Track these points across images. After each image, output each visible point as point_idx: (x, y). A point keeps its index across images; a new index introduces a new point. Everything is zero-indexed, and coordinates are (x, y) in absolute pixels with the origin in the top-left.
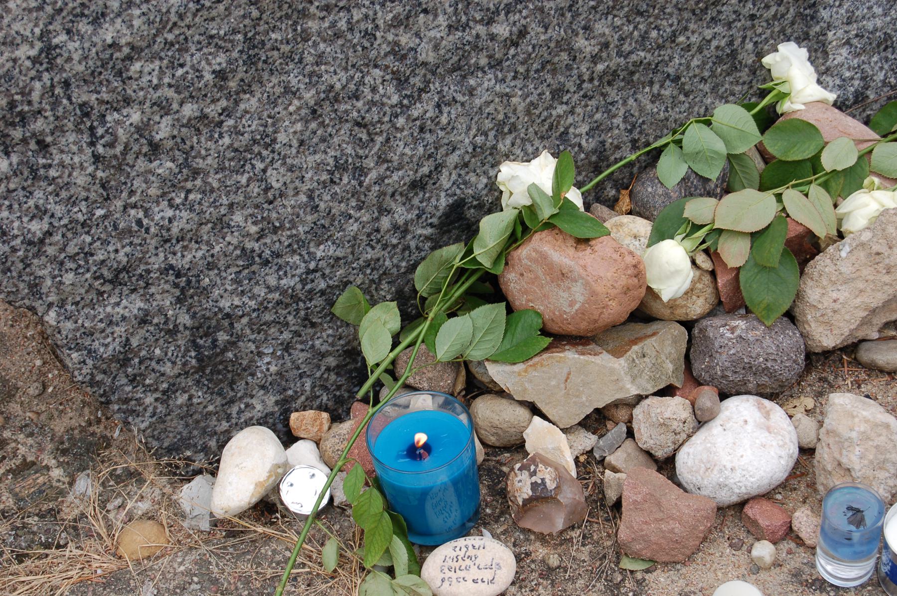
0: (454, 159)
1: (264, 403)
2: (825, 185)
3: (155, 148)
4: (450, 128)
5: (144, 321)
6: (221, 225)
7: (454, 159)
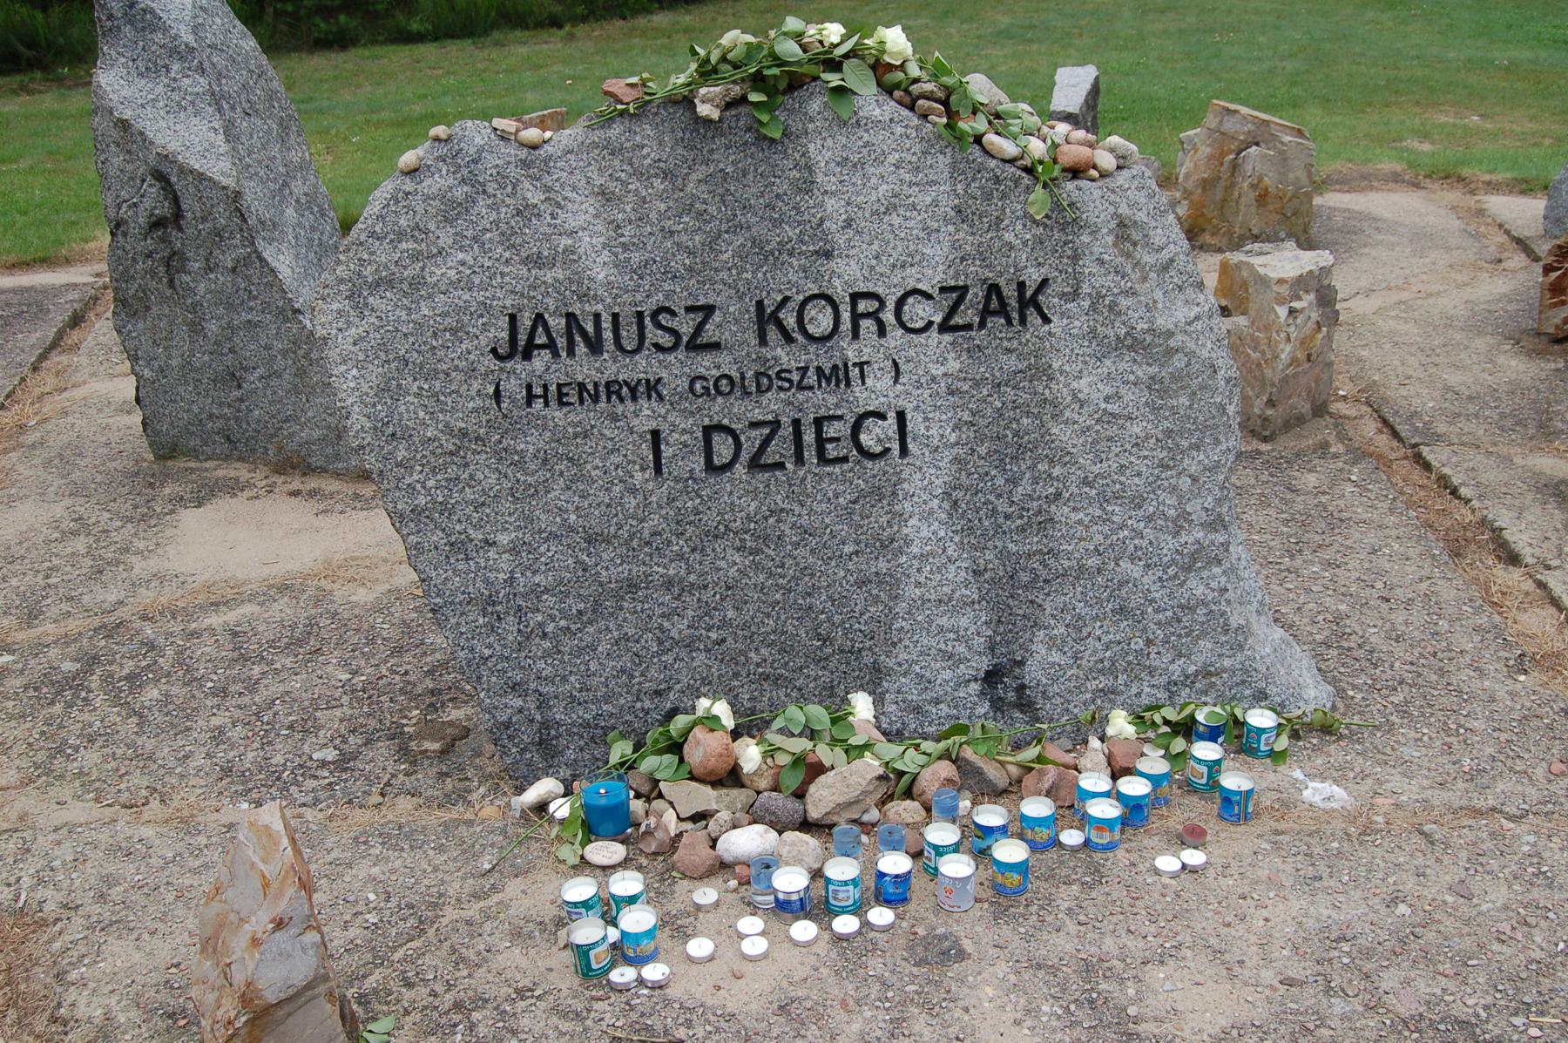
0: (678, 687)
1: (566, 772)
2: (846, 752)
3: (545, 635)
4: (678, 671)
5: (520, 711)
6: (564, 679)
7: (678, 687)
